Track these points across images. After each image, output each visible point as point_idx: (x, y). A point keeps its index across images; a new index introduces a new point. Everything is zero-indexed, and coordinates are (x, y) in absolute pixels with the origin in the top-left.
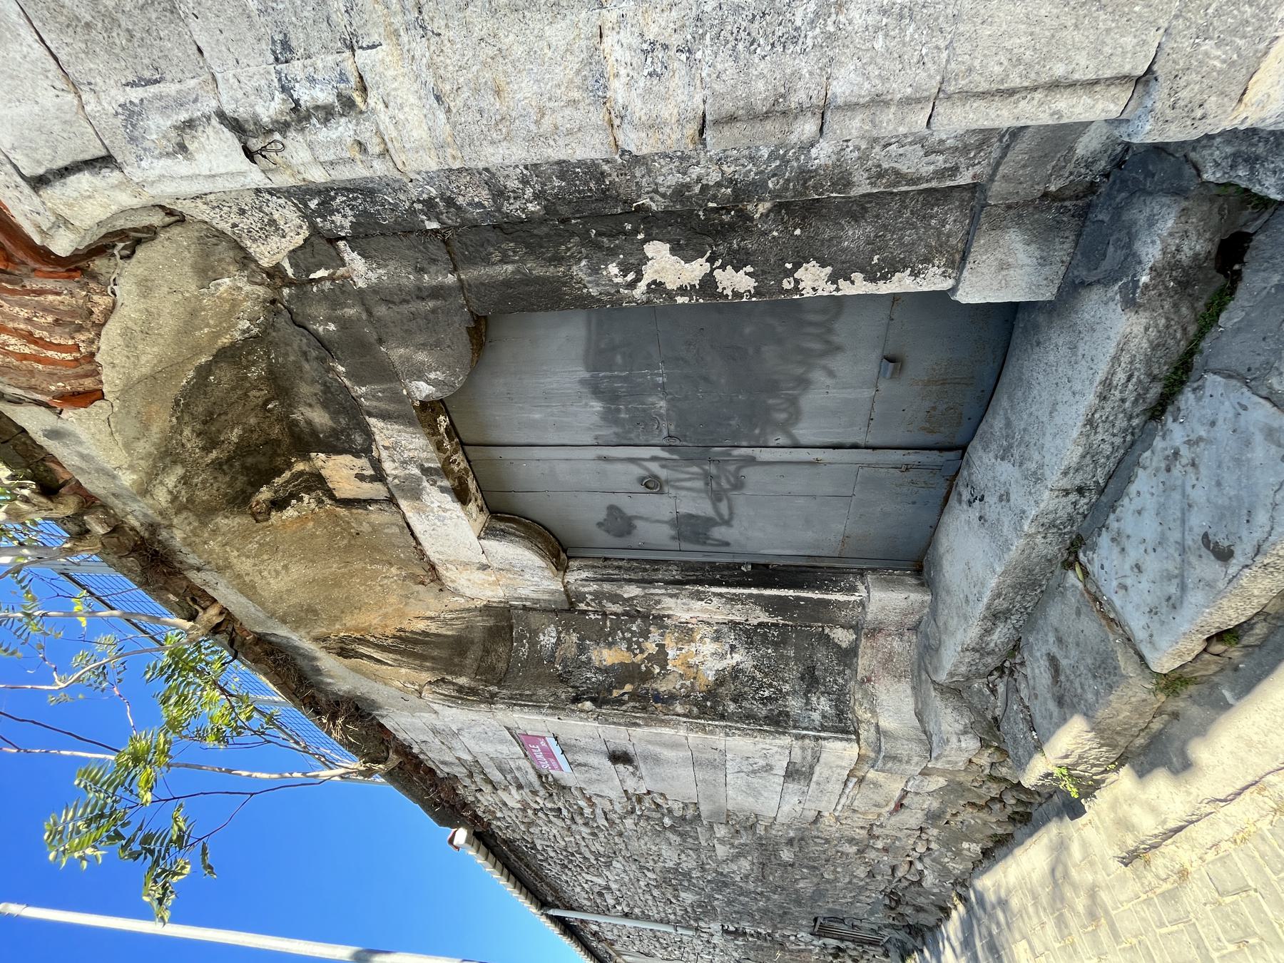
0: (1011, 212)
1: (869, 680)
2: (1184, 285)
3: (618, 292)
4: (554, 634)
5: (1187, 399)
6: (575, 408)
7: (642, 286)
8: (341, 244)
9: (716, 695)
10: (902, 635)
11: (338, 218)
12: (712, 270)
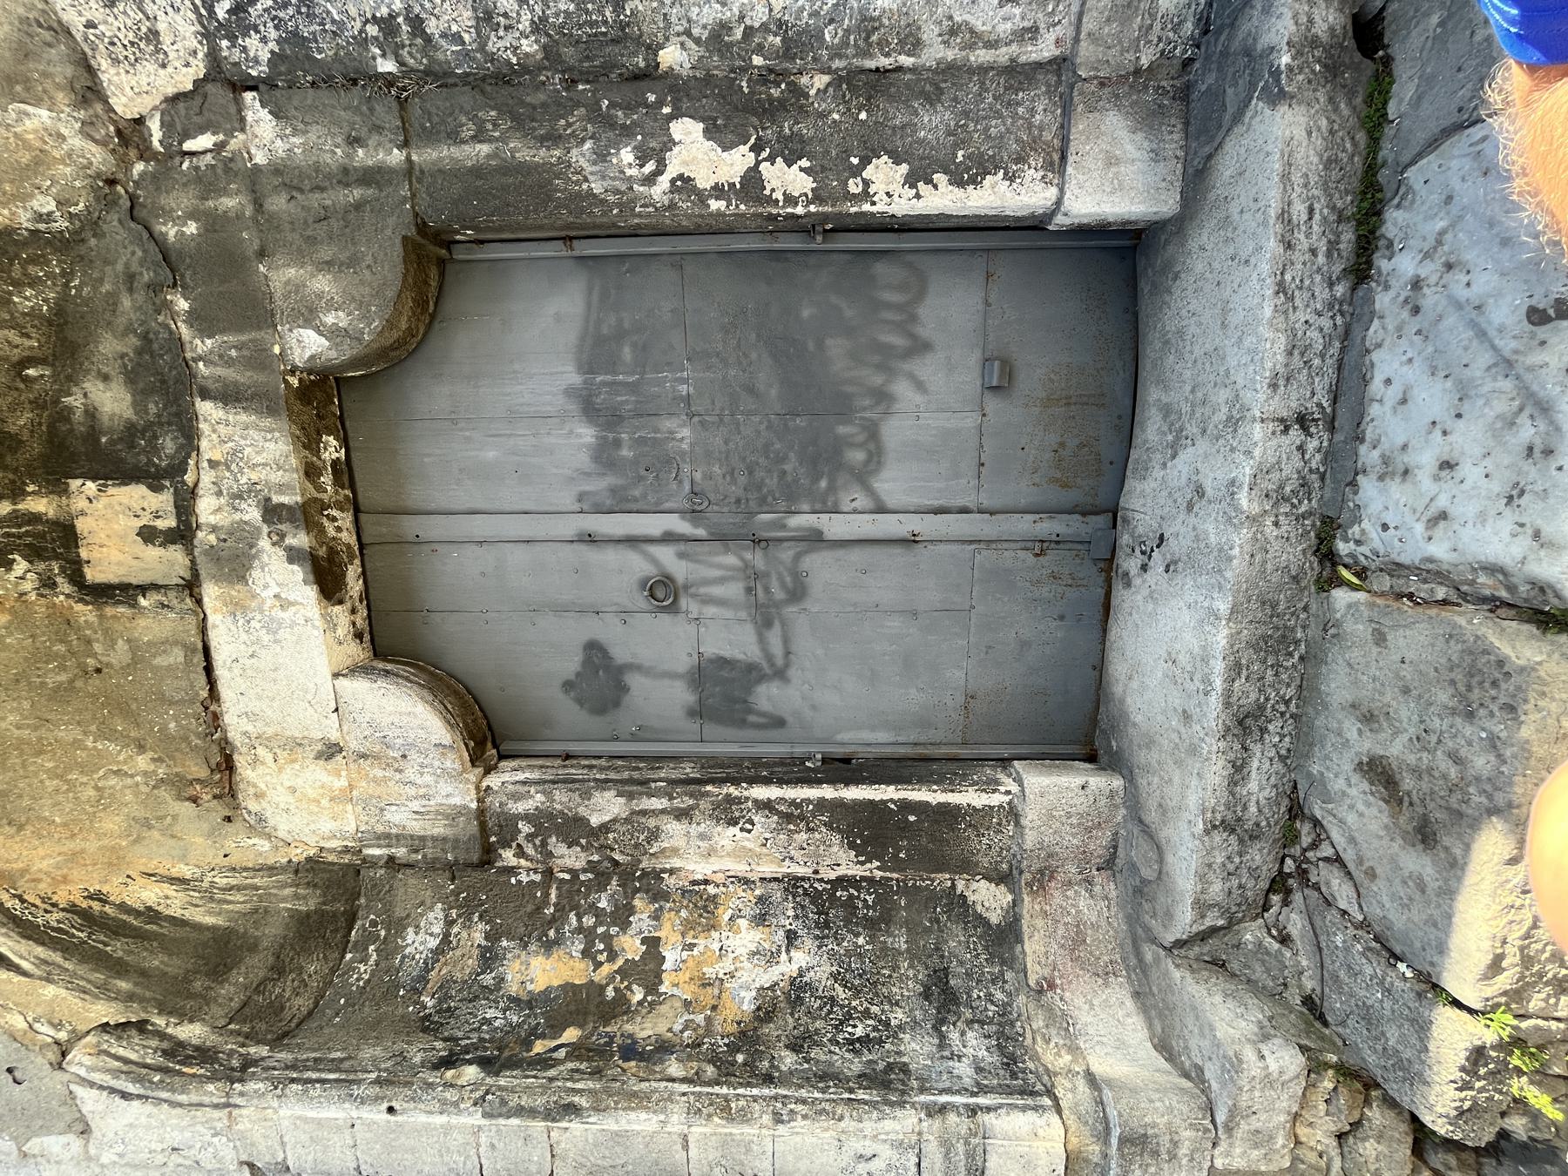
0: (1107, 90)
1: (1052, 986)
2: (1332, 70)
3: (631, 188)
4: (437, 929)
5: (1395, 220)
6: (553, 440)
7: (664, 182)
8: (249, 96)
9: (757, 1040)
10: (1089, 882)
11: (252, 42)
12: (758, 163)
